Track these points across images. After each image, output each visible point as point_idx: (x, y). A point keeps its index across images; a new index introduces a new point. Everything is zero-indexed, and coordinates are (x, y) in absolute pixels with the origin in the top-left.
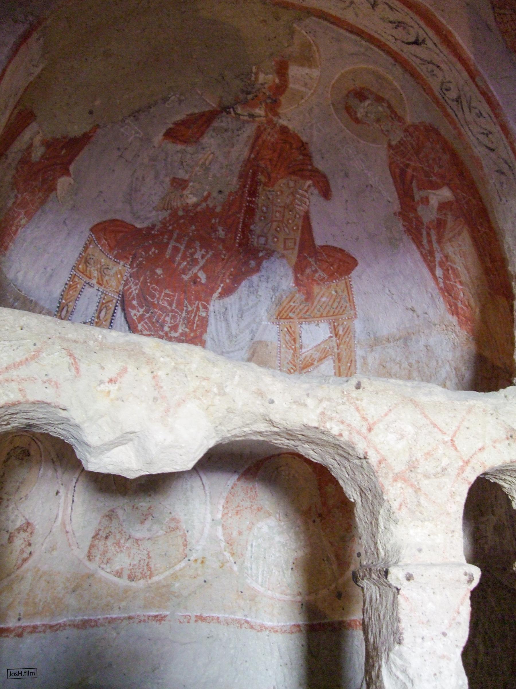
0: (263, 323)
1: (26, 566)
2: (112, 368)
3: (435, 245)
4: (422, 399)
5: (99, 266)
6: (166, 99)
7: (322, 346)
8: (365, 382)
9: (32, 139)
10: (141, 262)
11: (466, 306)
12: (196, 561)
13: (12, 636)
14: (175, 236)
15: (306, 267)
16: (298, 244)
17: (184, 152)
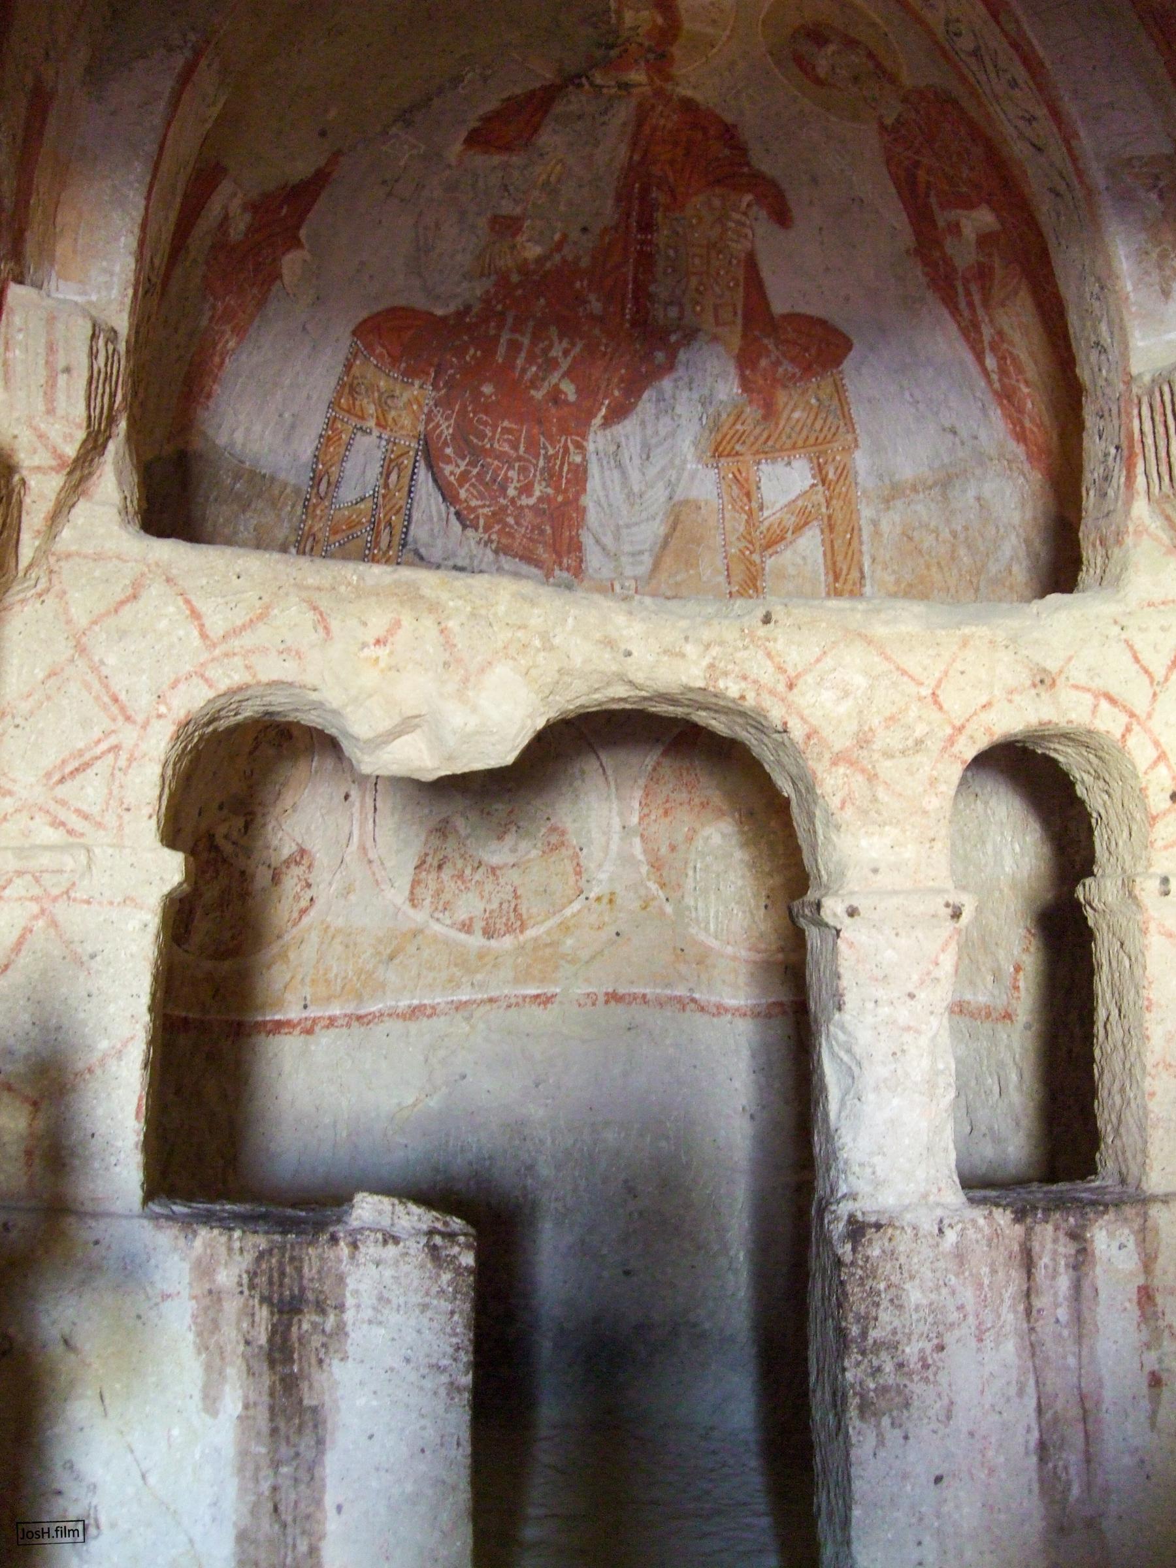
0: (689, 466)
1: (306, 920)
2: (378, 622)
3: (980, 312)
4: (880, 630)
5: (376, 394)
6: (457, 80)
7: (800, 503)
8: (778, 612)
9: (225, 208)
10: (452, 376)
11: (1037, 426)
12: (599, 899)
14: (510, 321)
15: (759, 356)
16: (740, 312)
17: (505, 166)
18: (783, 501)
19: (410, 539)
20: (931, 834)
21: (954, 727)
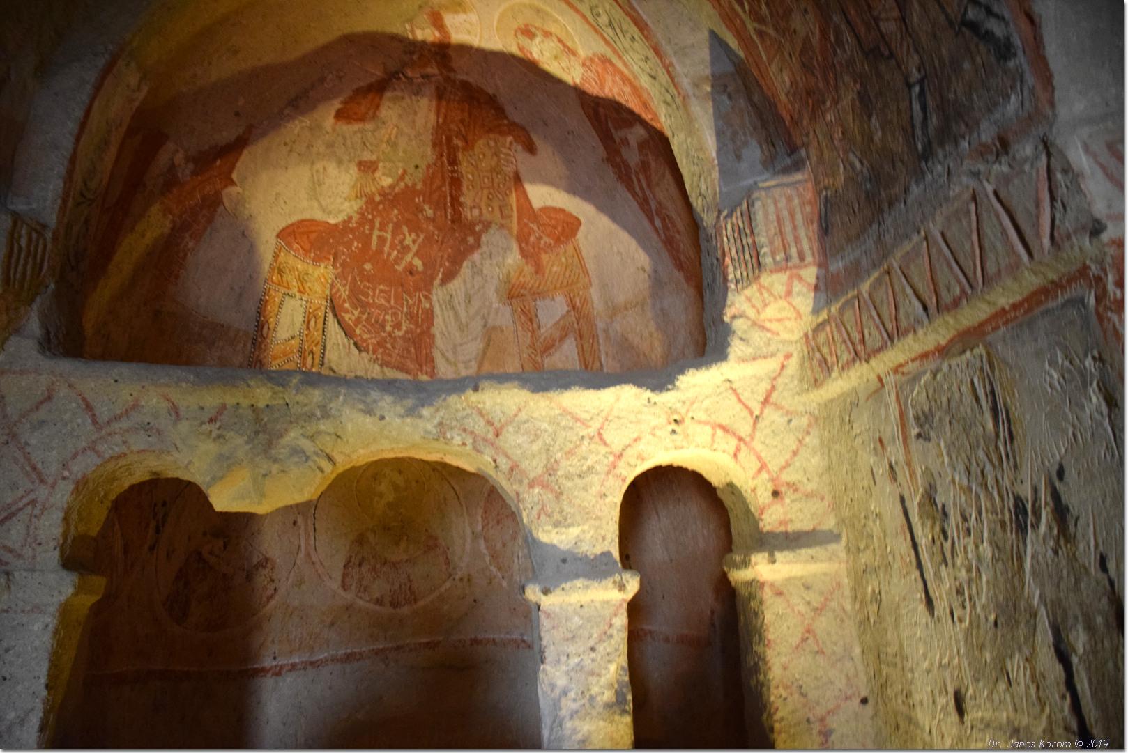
1: (273, 602)
6: (322, 80)
12: (461, 579)
13: (269, 675)
14: (377, 225)
18: (551, 322)
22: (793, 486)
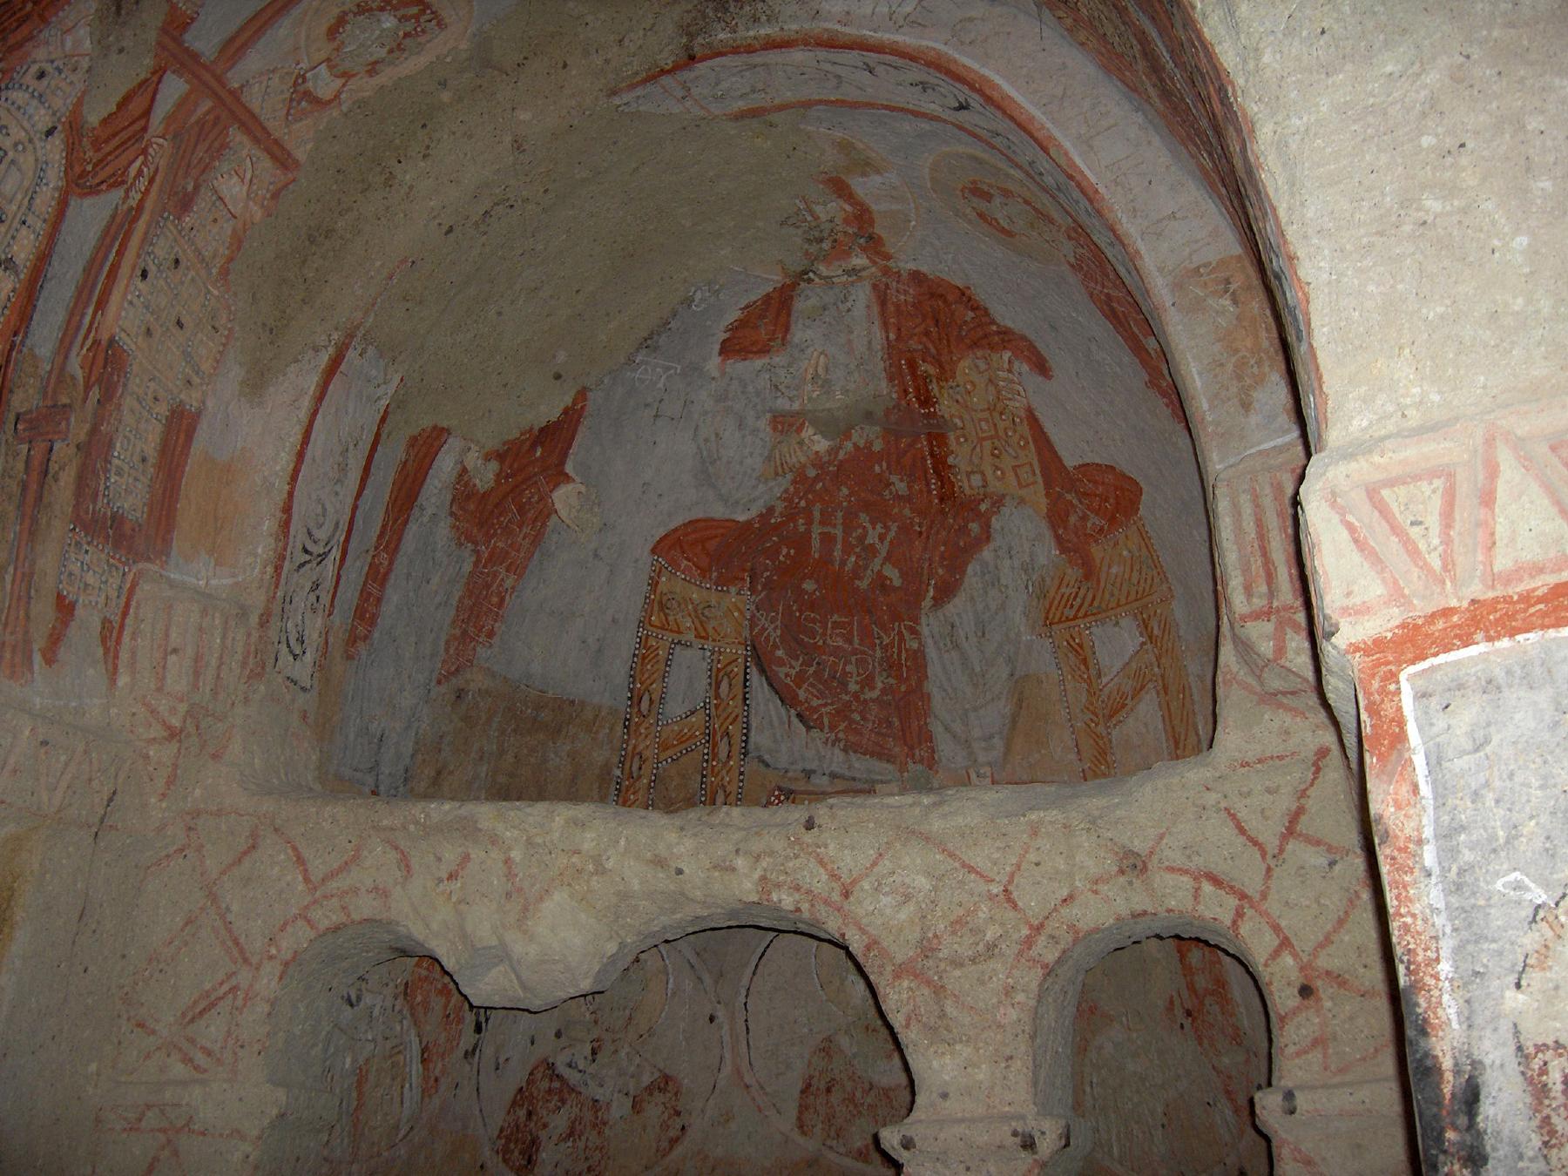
1: (679, 1150)
4: (936, 825)
14: (817, 515)
16: (1038, 472)
18: (1118, 665)
19: (751, 746)
20: (1008, 1052)
21: (1031, 927)
22: (1338, 979)
